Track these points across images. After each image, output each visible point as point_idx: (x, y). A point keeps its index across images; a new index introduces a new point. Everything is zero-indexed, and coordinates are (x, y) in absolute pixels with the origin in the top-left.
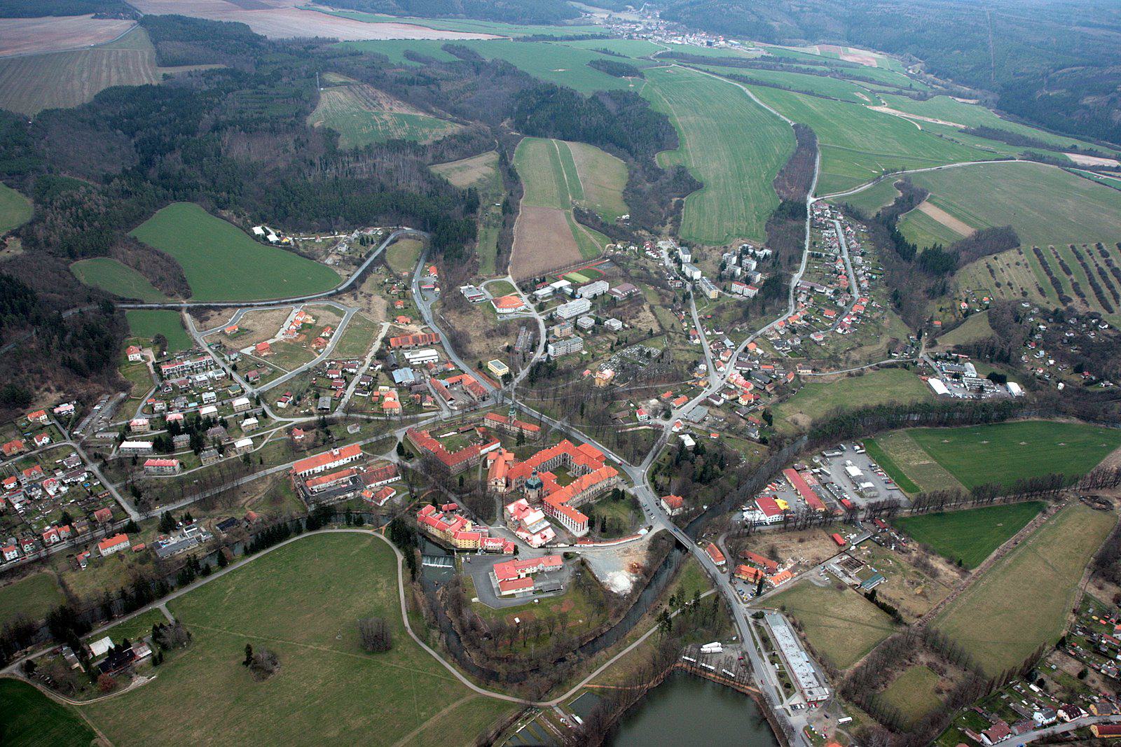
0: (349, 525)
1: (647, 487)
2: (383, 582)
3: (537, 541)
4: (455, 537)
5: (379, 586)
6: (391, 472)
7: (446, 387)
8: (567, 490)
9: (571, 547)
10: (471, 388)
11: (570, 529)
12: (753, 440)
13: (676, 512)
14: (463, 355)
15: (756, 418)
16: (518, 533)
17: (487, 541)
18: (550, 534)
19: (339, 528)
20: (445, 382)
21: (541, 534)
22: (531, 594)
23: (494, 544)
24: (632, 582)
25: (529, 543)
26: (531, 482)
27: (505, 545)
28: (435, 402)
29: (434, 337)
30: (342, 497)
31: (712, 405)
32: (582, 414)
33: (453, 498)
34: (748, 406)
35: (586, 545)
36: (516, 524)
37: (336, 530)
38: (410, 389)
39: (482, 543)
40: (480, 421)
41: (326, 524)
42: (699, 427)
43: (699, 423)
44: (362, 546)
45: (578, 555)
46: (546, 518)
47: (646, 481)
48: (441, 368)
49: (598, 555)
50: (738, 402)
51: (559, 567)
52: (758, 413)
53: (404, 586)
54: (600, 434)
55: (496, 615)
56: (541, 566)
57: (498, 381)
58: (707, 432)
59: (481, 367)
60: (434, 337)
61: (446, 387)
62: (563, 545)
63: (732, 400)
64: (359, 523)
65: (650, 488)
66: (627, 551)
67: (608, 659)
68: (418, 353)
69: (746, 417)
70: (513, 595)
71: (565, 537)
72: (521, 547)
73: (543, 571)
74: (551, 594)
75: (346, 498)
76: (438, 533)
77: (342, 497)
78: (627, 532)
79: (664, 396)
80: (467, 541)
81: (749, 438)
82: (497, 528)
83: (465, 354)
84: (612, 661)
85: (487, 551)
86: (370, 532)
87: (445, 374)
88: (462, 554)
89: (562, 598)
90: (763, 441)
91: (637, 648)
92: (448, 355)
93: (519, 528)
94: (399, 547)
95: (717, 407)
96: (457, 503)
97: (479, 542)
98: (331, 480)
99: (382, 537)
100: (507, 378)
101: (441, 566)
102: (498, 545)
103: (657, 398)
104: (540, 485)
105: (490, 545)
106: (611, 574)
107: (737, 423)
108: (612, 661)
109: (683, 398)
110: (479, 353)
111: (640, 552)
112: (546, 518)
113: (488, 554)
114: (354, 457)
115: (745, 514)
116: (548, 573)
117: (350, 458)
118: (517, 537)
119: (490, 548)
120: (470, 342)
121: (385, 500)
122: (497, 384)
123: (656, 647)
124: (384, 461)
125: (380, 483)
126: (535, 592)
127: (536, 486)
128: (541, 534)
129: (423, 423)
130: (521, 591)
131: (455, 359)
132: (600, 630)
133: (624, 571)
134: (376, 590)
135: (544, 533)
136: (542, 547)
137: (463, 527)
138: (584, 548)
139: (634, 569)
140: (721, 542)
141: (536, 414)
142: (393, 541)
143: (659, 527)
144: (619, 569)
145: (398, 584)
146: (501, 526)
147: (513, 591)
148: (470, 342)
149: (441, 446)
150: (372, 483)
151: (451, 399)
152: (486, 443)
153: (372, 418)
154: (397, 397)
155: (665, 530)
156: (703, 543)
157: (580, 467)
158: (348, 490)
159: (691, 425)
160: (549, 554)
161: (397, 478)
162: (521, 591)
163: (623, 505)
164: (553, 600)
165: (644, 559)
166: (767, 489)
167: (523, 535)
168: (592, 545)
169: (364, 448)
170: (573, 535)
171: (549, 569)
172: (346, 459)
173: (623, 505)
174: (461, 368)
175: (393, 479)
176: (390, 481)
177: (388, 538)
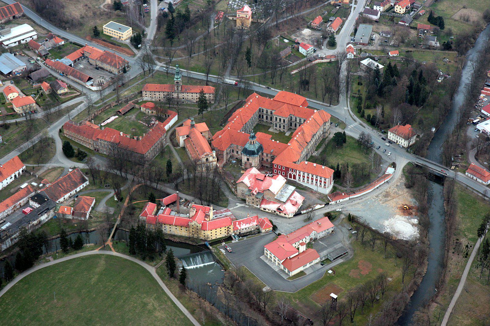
0: (66, 251)
1: (361, 124)
2: (152, 302)
3: (290, 209)
4: (203, 228)
5: (150, 307)
6: (76, 179)
7: (71, 65)
8: (293, 145)
9: (327, 207)
10: (103, 61)
11: (314, 187)
12: (434, 48)
13: (413, 141)
14: (64, 24)
15: (423, 23)
16: (263, 206)
17: (239, 224)
18: (299, 198)
19: (55, 258)
20: (67, 61)
21: (291, 201)
22: (320, 266)
23: (248, 226)
24: (413, 225)
25: (282, 214)
26: (251, 148)
27: (261, 223)
28: (69, 87)
29: (14, 9)
30: (35, 222)
31: (371, 22)
32: (249, 62)
33: (169, 190)
34: (408, 12)
35: (341, 200)
36: (260, 197)
37: (53, 262)
38: (29, 77)
39: (235, 228)
40: (136, 96)
41: (37, 258)
42: (370, 48)
43: (369, 44)
44: (98, 270)
45: (340, 213)
46: (289, 183)
47: (355, 117)
48: (49, 44)
49: (360, 207)
50: (394, 12)
51: (330, 230)
52: (421, 19)
53: (179, 298)
54: (277, 79)
55: (299, 298)
56: (313, 236)
57: (126, 46)
58: (383, 51)
59: (97, 34)
60: (14, 9)
61: (71, 65)
62: (318, 207)
63: (387, 11)
64: (78, 245)
65: (364, 124)
66: (387, 195)
67: (445, 310)
68: (9, 32)
69: (412, 25)
70: (302, 273)
71: (314, 198)
72: (276, 221)
73: (315, 240)
74: (340, 261)
75: (40, 222)
76: (182, 232)
77: (35, 222)
78: (372, 176)
79: (318, 21)
80: (214, 231)
81: (430, 48)
82: (235, 208)
83: (67, 22)
84: (450, 310)
85: (241, 235)
86: (96, 252)
87: (58, 52)
88: (218, 246)
89: (354, 262)
90: (447, 47)
91: (465, 290)
92: (44, 28)
93: (263, 201)
94: (144, 259)
95: (376, 21)
96: (174, 194)
97: (232, 227)
98: (7, 206)
99: (114, 253)
100: (137, 40)
101: (202, 265)
102: (252, 225)
103: (308, 27)
104: (261, 148)
105: (244, 227)
106: (386, 223)
107: (408, 34)
108: (450, 310)
109: (337, 21)
110: (82, 18)
111: (400, 193)
112: (289, 183)
113: (245, 238)
114: (17, 173)
115: (479, 127)
116: (322, 239)
117: (13, 175)
118: (264, 211)
119: (245, 231)
120: (63, 7)
121: (89, 212)
122: (127, 50)
123: (482, 283)
124: (54, 169)
125: (68, 194)
126: (322, 263)
127: (258, 151)
128: (291, 201)
129: (74, 112)
130: (308, 265)
131: (55, 31)
132: (415, 283)
133: (397, 216)
134: (150, 312)
135: (292, 198)
136: (297, 214)
137: (207, 216)
138: (341, 204)
139: (406, 211)
140: (473, 163)
141: (201, 76)
142: (132, 253)
143: (402, 162)
144: (392, 216)
145: (169, 298)
146: (239, 205)
147: (301, 269)
148: (63, 7)
149: (121, 133)
150: (60, 197)
151: (90, 79)
152: (162, 119)
153: (8, 122)
154: (19, 91)
155: (409, 164)
156: (456, 166)
157: (286, 120)
158: (38, 213)
159: (364, 48)
160: (309, 219)
161: (84, 185)
162: (308, 265)
163: (348, 149)
164: (347, 266)
165: (410, 199)
166: (482, 95)
167: (273, 207)
168: (348, 199)
169: (24, 158)
170: (320, 194)
171: (321, 235)
172: (9, 178)
173: (348, 149)
174: (73, 41)
175: (81, 187)
176: (78, 189)
177: (124, 252)
